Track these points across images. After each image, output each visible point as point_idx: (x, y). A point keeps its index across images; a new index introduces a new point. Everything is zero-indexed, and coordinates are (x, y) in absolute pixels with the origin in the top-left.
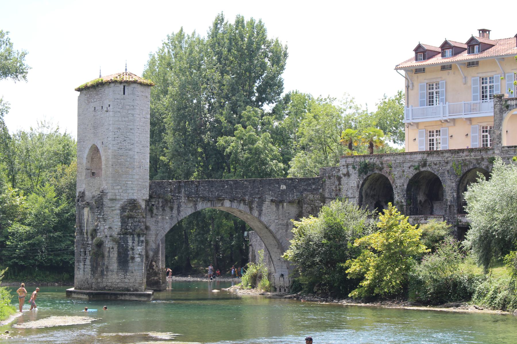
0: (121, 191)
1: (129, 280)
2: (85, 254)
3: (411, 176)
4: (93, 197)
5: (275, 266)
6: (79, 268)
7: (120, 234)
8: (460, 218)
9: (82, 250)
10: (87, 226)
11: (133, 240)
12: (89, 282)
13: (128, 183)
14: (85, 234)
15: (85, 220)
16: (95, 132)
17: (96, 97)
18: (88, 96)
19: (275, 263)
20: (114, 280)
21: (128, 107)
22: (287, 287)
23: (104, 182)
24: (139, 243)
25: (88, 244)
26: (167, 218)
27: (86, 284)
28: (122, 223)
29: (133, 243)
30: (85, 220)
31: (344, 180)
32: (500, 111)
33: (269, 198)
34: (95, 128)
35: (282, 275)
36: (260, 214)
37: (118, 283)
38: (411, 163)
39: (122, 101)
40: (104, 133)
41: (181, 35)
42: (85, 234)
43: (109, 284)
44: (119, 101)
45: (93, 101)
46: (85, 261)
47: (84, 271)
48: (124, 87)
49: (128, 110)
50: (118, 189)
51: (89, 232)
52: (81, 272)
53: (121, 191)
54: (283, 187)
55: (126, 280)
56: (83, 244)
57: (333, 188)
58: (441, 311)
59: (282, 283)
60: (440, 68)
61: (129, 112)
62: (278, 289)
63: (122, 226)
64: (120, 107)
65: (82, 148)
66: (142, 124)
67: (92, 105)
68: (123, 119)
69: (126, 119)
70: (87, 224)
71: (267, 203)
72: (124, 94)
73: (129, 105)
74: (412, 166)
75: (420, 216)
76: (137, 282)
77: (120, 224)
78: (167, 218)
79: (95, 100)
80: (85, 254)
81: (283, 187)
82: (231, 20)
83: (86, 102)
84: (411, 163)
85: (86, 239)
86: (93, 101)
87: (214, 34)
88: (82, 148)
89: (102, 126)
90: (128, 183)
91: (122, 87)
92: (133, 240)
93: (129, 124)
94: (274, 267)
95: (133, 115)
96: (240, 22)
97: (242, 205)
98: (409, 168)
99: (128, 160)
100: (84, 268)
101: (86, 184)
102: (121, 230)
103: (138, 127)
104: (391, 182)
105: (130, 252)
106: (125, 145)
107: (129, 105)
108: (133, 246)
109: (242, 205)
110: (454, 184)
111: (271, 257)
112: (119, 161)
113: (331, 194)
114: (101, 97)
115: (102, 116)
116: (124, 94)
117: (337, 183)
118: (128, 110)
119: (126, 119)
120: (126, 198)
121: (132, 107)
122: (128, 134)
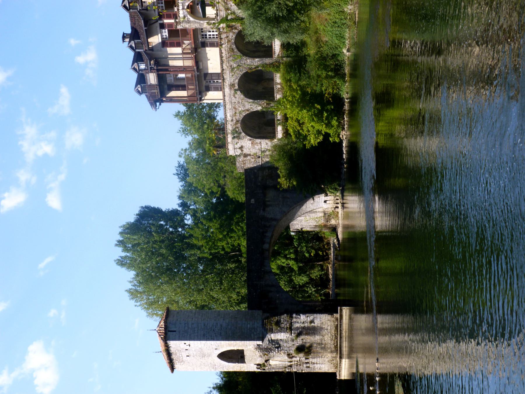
0: (255, 333)
1: (328, 326)
2: (308, 363)
3: (242, 96)
4: (261, 356)
5: (317, 207)
6: (320, 369)
7: (291, 333)
8: (276, 55)
9: (305, 366)
10: (285, 362)
11: (296, 322)
12: (332, 360)
13: (248, 327)
14: (291, 363)
15: (280, 363)
16: (207, 355)
17: (178, 355)
18: (177, 361)
19: (315, 208)
20: (329, 339)
21: (186, 328)
22: (335, 198)
23: (249, 348)
25: (300, 360)
26: (278, 295)
27: (333, 361)
28: (282, 332)
29: (298, 322)
30: (280, 363)
31: (246, 151)
32: (188, 23)
33: (262, 213)
34: (204, 356)
35: (325, 202)
37: (331, 335)
38: (232, 97)
39: (181, 333)
41: (129, 291)
42: (291, 363)
43: (332, 342)
44: (181, 336)
45: (181, 358)
46: (314, 363)
47: (322, 364)
48: (169, 331)
49: (188, 328)
50: (254, 335)
51: (290, 360)
52: (323, 366)
53: (255, 333)
54: (253, 201)
55: (329, 328)
56: (300, 365)
57: (253, 160)
58: (471, 264)
59: (331, 202)
60: (314, 349)
61: (191, 327)
62: (336, 205)
64: (186, 334)
65: (221, 366)
66: (200, 317)
67: (185, 358)
68: (196, 332)
69: (196, 329)
71: (265, 214)
73: (185, 327)
74: (234, 96)
75: (275, 88)
76: (330, 319)
78: (278, 295)
79: (181, 356)
80: (308, 363)
82: (119, 252)
83: (182, 363)
84: (232, 97)
85: (296, 362)
86: (181, 358)
87: (130, 266)
88: (221, 366)
89: (202, 349)
90: (248, 327)
91: (169, 333)
92: (296, 322)
93: (200, 328)
94: (319, 208)
95: (192, 324)
96: (121, 243)
97: (267, 234)
98: (235, 97)
99: (229, 327)
100: (320, 364)
101: (250, 363)
102: (288, 332)
103: (203, 319)
104: (248, 112)
105: (306, 325)
106: (217, 330)
107: (185, 327)
108: (301, 322)
109: (267, 234)
111: (309, 212)
112: (230, 335)
114: (178, 351)
115: (193, 349)
117: (249, 157)
118: (188, 328)
119: (196, 329)
120: (261, 329)
121: (186, 325)
122: (208, 328)
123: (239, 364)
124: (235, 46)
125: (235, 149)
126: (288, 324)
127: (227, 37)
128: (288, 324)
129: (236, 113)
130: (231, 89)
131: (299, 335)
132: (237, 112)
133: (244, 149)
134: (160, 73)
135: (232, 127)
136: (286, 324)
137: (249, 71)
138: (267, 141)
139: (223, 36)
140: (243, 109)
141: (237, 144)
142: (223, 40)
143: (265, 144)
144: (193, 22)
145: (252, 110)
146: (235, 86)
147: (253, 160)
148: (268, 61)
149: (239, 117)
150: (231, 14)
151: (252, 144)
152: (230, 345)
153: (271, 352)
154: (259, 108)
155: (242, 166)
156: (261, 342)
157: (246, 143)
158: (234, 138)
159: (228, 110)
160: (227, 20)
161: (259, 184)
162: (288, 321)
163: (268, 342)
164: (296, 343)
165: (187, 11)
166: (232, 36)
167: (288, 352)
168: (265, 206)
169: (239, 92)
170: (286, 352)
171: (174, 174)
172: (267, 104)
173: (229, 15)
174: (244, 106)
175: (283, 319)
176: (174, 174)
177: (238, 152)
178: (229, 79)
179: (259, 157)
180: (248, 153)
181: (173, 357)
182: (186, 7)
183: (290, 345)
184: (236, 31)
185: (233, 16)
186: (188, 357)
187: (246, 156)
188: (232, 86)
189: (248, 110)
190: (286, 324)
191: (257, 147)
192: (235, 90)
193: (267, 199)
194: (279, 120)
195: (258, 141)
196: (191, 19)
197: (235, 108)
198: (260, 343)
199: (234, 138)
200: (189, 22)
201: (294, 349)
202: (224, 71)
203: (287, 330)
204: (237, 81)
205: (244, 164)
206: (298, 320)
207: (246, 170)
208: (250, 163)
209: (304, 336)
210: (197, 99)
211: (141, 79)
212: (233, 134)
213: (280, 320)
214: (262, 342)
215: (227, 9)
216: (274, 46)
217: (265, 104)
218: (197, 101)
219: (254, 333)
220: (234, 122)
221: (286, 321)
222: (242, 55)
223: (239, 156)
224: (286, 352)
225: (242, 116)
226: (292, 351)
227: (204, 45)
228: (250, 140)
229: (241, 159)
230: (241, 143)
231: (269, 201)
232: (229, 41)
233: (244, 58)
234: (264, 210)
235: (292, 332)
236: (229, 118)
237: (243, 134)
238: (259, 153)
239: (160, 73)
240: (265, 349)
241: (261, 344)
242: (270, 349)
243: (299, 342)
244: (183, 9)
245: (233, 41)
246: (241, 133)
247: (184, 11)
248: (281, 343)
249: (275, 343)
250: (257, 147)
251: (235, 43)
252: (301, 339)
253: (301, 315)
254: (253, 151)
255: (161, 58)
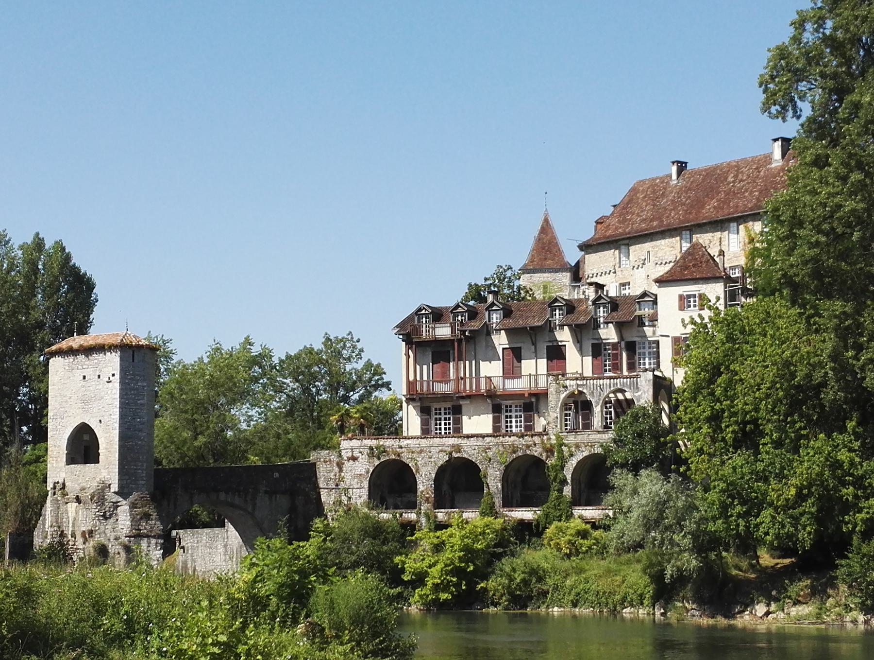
0: (129, 481)
3: (440, 463)
7: (129, 537)
11: (149, 543)
24: (157, 547)
28: (131, 522)
29: (149, 546)
31: (348, 465)
36: (254, 509)
38: (440, 448)
40: (104, 409)
53: (129, 481)
57: (332, 475)
63: (132, 525)
70: (73, 524)
72: (133, 361)
74: (441, 451)
77: (129, 523)
81: (276, 475)
84: (440, 448)
86: (80, 367)
92: (149, 543)
97: (236, 497)
109: (236, 497)
110: (498, 473)
113: (327, 484)
114: (98, 364)
116: (133, 361)
117: (337, 469)
123: (65, 456)
124: (520, 454)
125: (352, 449)
126: (145, 531)
127: (535, 445)
128: (145, 531)
129: (413, 452)
130: (453, 446)
131: (127, 549)
132: (415, 455)
133: (351, 462)
134: (456, 344)
135: (389, 447)
136: (145, 529)
137: (482, 473)
138: (365, 497)
139: (537, 439)
140: (419, 463)
141: (361, 452)
142: (530, 439)
143: (360, 495)
144: (559, 398)
145: (417, 476)
146: (457, 452)
147: (332, 475)
148: (498, 501)
149: (406, 458)
150: (570, 451)
151: (361, 475)
152: (109, 443)
153: (97, 506)
154: (421, 487)
155: (322, 460)
156: (117, 490)
157: (364, 467)
158: (371, 448)
159: (418, 442)
160: (561, 445)
161: (298, 485)
162: (151, 531)
163: (114, 500)
164: (113, 543)
165: (574, 390)
166: (537, 451)
167: (96, 531)
168: (271, 493)
169: (447, 458)
170: (97, 528)
171: (150, 332)
172: (427, 499)
173: (569, 448)
174: (425, 464)
175: (155, 524)
176: (150, 332)
177: (345, 454)
178: (468, 444)
179: (337, 485)
180: (344, 469)
181: (81, 358)
182: (580, 389)
183: (108, 535)
184: (544, 458)
185: (566, 454)
186: (82, 378)
187: (340, 465)
188: (458, 449)
189: (417, 470)
190: (145, 529)
191: (355, 483)
192: (451, 453)
193: (278, 496)
194: (401, 515)
195: (366, 484)
196: (563, 396)
197: (421, 452)
198: (115, 487)
199: (371, 448)
200: (558, 392)
201: (103, 540)
202: (481, 439)
203: (136, 530)
204: (465, 456)
205: (325, 462)
206: (153, 546)
207: (314, 465)
208: (325, 473)
209: (125, 555)
210: (413, 395)
211: (437, 315)
212: (377, 448)
213: (152, 520)
214: (115, 493)
215: (577, 446)
216: (521, 509)
217: (428, 496)
218: (410, 395)
219: (130, 479)
220: (398, 450)
221: (151, 528)
222: (506, 464)
223: (340, 456)
224: (97, 528)
225: (407, 462)
226: (98, 538)
227: (497, 410)
228: (368, 473)
229: (334, 458)
230: (363, 459)
231: (276, 497)
232: (528, 447)
233: (502, 468)
234: (266, 492)
235: (132, 537)
236: (404, 443)
237: (377, 462)
238: (342, 485)
239: (456, 344)
240: (104, 496)
241: (112, 490)
242: (103, 504)
243: (113, 548)
244: (578, 385)
245: (528, 452)
246: (379, 459)
247: (575, 387)
248: (112, 520)
249: (113, 511)
250: (355, 483)
251: (526, 456)
252: (121, 551)
253: (162, 551)
254: (347, 475)
255: (475, 344)
